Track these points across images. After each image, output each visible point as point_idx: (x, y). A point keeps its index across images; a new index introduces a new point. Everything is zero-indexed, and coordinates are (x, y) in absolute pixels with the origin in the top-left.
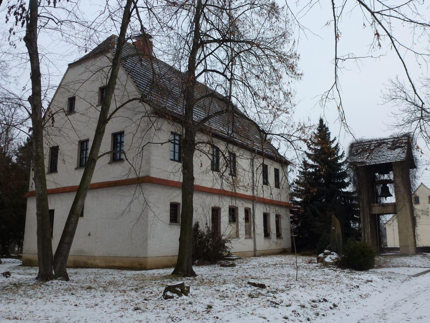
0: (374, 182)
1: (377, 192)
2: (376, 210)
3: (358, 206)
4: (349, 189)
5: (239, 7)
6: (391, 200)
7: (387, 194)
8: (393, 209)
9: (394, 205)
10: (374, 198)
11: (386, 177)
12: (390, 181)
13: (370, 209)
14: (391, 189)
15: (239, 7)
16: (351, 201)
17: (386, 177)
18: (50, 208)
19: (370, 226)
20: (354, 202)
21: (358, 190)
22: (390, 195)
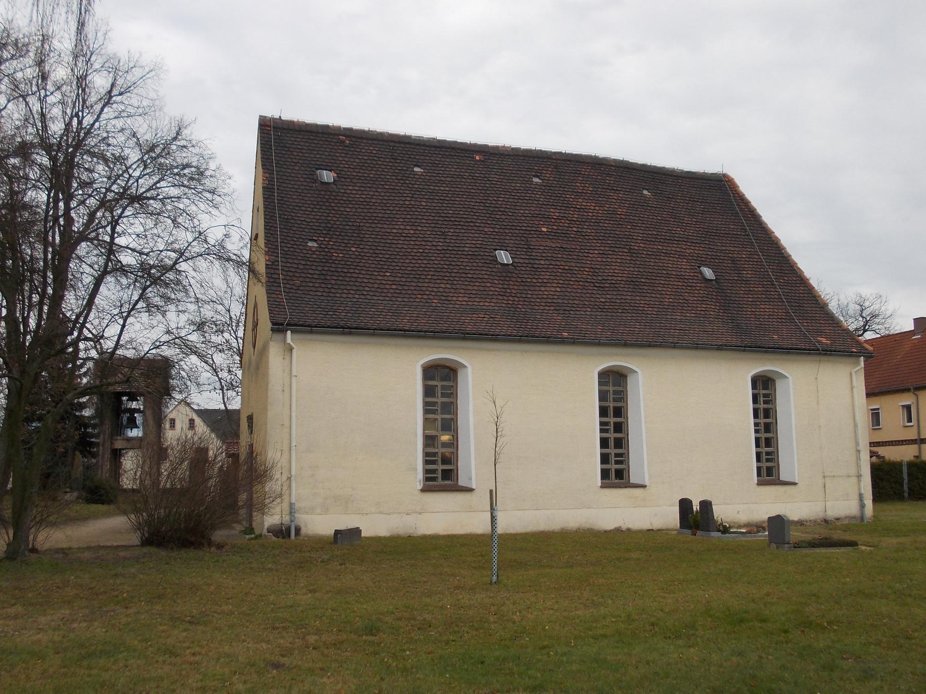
0: (118, 410)
1: (122, 423)
2: (119, 444)
3: (97, 436)
4: (87, 413)
5: (123, 326)
6: (135, 433)
7: (132, 424)
8: (137, 444)
9: (140, 439)
10: (118, 429)
11: (134, 405)
12: (138, 411)
13: (112, 443)
14: (139, 418)
15: (123, 326)
16: (85, 429)
17: (134, 405)
18: (670, 517)
19: (469, 446)
20: (90, 430)
21: (99, 414)
22: (137, 427)
